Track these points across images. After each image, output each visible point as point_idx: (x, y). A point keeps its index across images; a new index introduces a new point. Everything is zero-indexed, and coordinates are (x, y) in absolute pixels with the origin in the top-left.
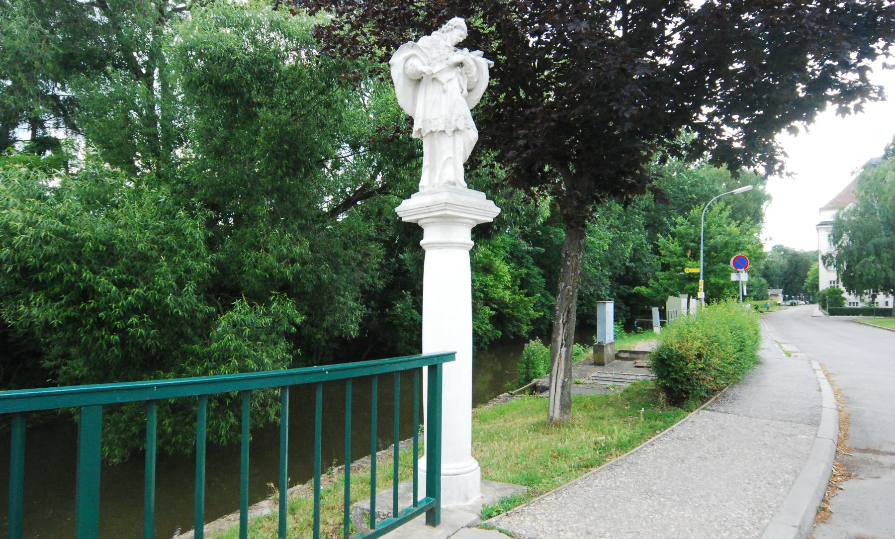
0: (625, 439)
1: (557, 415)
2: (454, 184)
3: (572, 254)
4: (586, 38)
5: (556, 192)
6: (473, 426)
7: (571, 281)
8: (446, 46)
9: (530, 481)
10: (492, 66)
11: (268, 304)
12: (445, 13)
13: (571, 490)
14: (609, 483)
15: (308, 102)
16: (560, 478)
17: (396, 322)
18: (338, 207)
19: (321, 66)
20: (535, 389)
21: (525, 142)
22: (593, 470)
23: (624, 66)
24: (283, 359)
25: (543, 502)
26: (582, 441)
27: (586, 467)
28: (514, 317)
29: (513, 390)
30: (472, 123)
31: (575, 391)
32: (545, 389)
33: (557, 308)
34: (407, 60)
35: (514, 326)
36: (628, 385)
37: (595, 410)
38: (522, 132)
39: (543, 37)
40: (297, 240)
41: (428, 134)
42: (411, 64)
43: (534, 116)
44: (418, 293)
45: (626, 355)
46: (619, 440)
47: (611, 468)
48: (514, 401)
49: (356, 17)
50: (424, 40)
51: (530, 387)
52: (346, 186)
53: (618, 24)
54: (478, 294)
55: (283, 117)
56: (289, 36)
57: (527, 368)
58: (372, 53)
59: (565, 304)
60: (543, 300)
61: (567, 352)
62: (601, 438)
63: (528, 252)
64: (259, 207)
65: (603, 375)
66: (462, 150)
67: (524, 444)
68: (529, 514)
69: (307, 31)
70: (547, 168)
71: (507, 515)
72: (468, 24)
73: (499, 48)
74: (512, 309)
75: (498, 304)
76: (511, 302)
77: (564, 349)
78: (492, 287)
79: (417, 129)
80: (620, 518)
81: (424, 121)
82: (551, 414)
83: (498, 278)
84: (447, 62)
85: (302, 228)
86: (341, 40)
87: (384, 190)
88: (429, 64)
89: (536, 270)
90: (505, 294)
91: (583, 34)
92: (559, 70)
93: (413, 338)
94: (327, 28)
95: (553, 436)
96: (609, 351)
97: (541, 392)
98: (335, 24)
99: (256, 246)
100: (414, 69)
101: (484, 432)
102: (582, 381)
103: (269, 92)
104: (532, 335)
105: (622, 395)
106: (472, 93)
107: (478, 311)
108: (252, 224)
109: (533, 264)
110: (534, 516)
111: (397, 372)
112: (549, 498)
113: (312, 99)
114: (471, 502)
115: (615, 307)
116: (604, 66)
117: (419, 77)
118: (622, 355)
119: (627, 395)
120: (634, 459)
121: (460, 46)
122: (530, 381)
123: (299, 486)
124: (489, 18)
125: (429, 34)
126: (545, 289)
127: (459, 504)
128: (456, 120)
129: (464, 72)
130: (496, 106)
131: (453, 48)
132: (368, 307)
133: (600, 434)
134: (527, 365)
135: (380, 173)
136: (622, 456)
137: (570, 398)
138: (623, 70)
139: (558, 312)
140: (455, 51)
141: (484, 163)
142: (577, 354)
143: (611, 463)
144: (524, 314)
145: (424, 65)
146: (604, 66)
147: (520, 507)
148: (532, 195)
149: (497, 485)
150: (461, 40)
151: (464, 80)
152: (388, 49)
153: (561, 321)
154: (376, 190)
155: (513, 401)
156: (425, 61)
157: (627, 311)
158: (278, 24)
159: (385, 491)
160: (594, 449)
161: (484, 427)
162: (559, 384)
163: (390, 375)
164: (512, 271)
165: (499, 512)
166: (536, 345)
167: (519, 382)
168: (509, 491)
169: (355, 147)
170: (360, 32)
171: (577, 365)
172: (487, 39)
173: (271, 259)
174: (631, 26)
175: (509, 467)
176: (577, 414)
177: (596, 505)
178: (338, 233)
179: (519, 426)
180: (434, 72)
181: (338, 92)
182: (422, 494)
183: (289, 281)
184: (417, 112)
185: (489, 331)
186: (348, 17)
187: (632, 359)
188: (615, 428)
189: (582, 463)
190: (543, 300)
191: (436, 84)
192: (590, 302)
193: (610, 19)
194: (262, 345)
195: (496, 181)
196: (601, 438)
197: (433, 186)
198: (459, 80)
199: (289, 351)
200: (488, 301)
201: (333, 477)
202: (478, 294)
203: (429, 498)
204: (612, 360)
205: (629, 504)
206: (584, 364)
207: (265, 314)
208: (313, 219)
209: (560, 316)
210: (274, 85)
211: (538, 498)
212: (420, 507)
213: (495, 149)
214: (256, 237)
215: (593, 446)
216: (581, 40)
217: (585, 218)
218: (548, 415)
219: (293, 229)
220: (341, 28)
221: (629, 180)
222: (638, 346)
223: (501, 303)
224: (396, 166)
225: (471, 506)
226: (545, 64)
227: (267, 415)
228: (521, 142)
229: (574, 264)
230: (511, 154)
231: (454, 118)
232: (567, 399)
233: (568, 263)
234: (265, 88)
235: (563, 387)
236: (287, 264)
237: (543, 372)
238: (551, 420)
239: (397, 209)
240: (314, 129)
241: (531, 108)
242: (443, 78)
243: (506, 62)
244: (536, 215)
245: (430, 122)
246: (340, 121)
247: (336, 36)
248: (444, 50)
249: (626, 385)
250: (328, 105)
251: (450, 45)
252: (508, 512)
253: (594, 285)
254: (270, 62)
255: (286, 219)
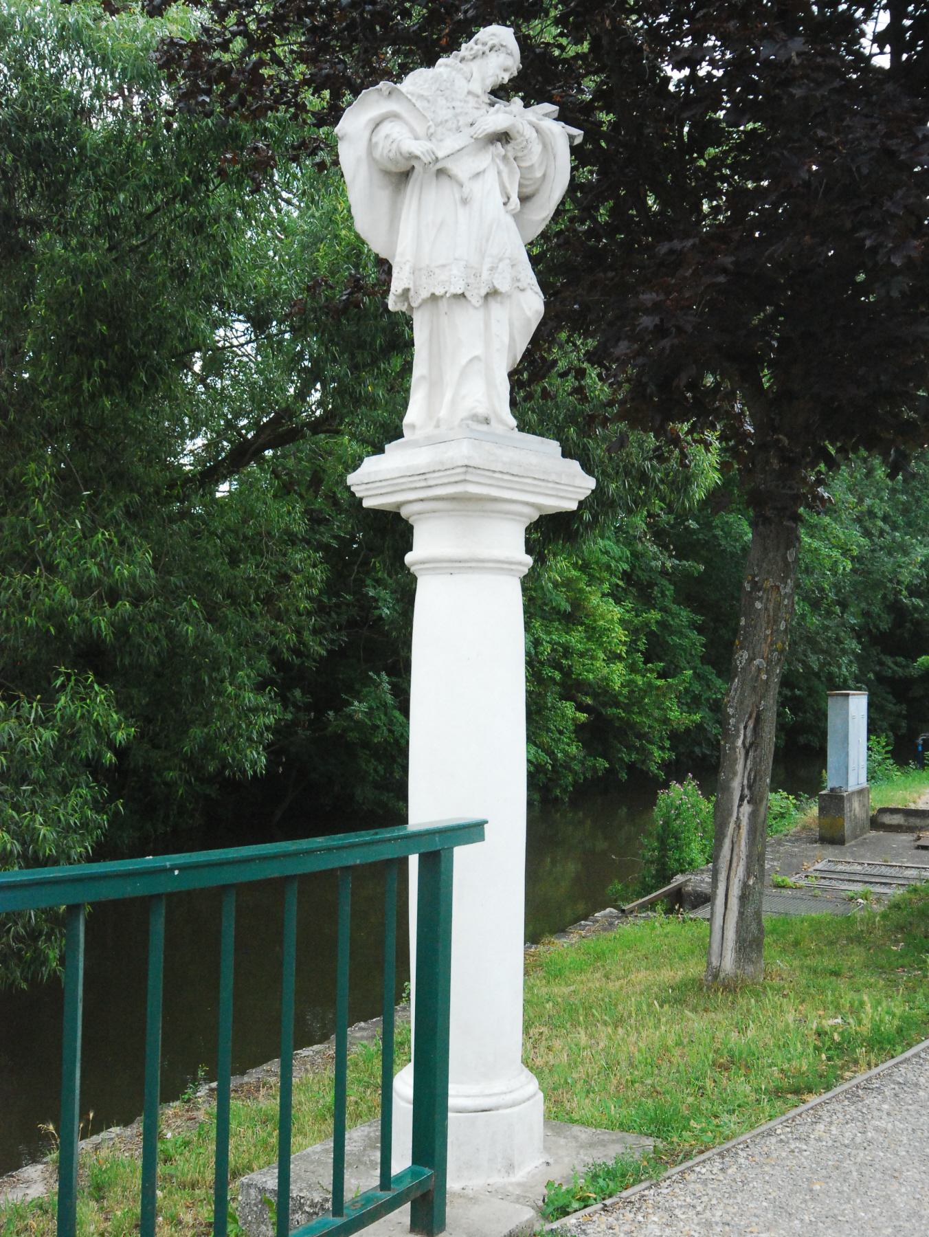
0: (890, 1025)
1: (728, 964)
2: (487, 421)
3: (768, 584)
4: (802, 77)
5: (732, 434)
6: (528, 988)
7: (765, 648)
8: (469, 93)
9: (660, 1125)
10: (578, 141)
11: (49, 700)
12: (471, 13)
13: (757, 1150)
14: (851, 1131)
15: (149, 216)
16: (734, 1118)
17: (353, 736)
18: (219, 464)
19: (179, 133)
20: (680, 901)
21: (657, 320)
22: (813, 1100)
23: (893, 143)
24: (85, 824)
25: (693, 1177)
26: (787, 1029)
27: (797, 1091)
28: (631, 726)
29: (628, 900)
30: (528, 276)
31: (771, 907)
32: (703, 899)
33: (731, 711)
34: (377, 125)
35: (630, 748)
36: (901, 891)
37: (821, 952)
38: (648, 297)
39: (704, 70)
40: (122, 543)
41: (425, 301)
42: (387, 136)
43: (676, 261)
44: (400, 669)
45: (897, 819)
46: (876, 1029)
47: (853, 1096)
48: (628, 928)
49: (260, 20)
50: (418, 80)
51: (668, 895)
52: (237, 416)
53: (879, 39)
54: (548, 672)
55: (92, 256)
56: (103, 61)
57: (663, 847)
58: (297, 105)
59: (749, 702)
60: (697, 688)
61: (753, 815)
62: (831, 1022)
63: (664, 572)
64: (33, 466)
65: (840, 867)
66: (506, 340)
67: (651, 1035)
68: (657, 1207)
69: (146, 49)
70: (709, 380)
71: (605, 1209)
72: (523, 40)
73: (598, 94)
74: (627, 708)
75: (595, 696)
76: (625, 691)
77: (746, 809)
78: (582, 655)
79: (400, 291)
80: (875, 1218)
81: (413, 272)
82: (715, 963)
83: (594, 634)
84: (472, 131)
85: (131, 515)
86: (226, 74)
87: (327, 424)
88: (430, 137)
89: (685, 615)
90: (612, 672)
91: (794, 66)
92: (740, 148)
93: (391, 773)
94: (191, 44)
95: (720, 1016)
96: (855, 809)
97: (695, 907)
98: (210, 37)
99: (24, 559)
100: (394, 146)
101: (556, 1004)
102: (790, 881)
103: (57, 195)
104: (675, 771)
105: (884, 916)
106: (529, 205)
107: (546, 713)
108: (16, 506)
109: (675, 601)
110: (669, 1210)
111: (346, 869)
112: (706, 1169)
113: (157, 210)
114: (520, 1175)
115: (870, 705)
116: (844, 143)
117: (404, 167)
118: (888, 819)
119: (894, 915)
120: (910, 1075)
121: (500, 92)
122: (668, 880)
123: (115, 1130)
124: (573, 26)
125: (430, 62)
126: (705, 659)
127: (491, 1181)
128: (492, 269)
129: (511, 155)
130: (589, 233)
131: (486, 98)
132: (285, 702)
133: (831, 1012)
134: (662, 841)
135: (318, 386)
136: (882, 1067)
137: (759, 923)
138: (891, 154)
139: (732, 721)
140: (492, 105)
141: (562, 365)
142: (782, 816)
143: (854, 1082)
144: (656, 720)
145: (416, 138)
146: (844, 143)
147: (637, 1188)
148: (675, 441)
149: (584, 1134)
150: (506, 78)
151: (511, 172)
152: (337, 96)
153: (739, 742)
154: (307, 425)
155: (627, 927)
156: (420, 130)
157: (899, 715)
158: (79, 33)
159: (318, 1147)
160: (816, 1048)
161: (556, 990)
162: (735, 891)
163: (328, 877)
164: (627, 616)
165: (585, 1202)
166: (685, 793)
167: (643, 883)
168: (610, 1152)
169: (259, 323)
170: (267, 57)
171: (779, 843)
172: (571, 72)
173: (62, 591)
174: (911, 46)
175: (612, 1089)
176: (778, 962)
177: (817, 1187)
178: (219, 528)
179: (638, 989)
180: (440, 155)
181: (220, 195)
182: (402, 1160)
183: (104, 641)
184: (399, 250)
185: (574, 758)
186: (241, 21)
187: (910, 829)
188: (866, 998)
189: (785, 1083)
190: (697, 688)
191: (444, 181)
192: (811, 691)
193: (863, 26)
194: (33, 792)
195: (587, 408)
196: (831, 1022)
197: (437, 426)
198: (499, 173)
199: (98, 807)
200: (572, 688)
201: (198, 1109)
202: (548, 672)
203: (418, 1168)
204: (863, 832)
205: (896, 1186)
206: (797, 839)
207: (40, 722)
208: (157, 493)
209: (738, 730)
210: (67, 178)
211: (679, 1168)
212: (397, 1189)
213: (587, 335)
214: (25, 536)
215: (812, 1040)
216: (787, 83)
217: (798, 499)
218: (709, 963)
219: (113, 516)
220: (225, 46)
221: (907, 414)
222: (924, 798)
223: (603, 692)
224: (355, 367)
225: (519, 1184)
226: (708, 133)
227: (42, 960)
228: (647, 321)
229: (771, 606)
230: (623, 348)
231: (486, 267)
232: (754, 927)
233: (758, 605)
234: (48, 185)
235: (743, 898)
236: (100, 598)
237: (700, 859)
238: (716, 976)
239: (351, 479)
240: (164, 284)
241: (671, 239)
242: (462, 169)
243: (614, 126)
244: (688, 480)
245: (430, 274)
246: (227, 265)
247: (212, 65)
248: (466, 102)
249: (896, 893)
250: (197, 227)
251: (479, 91)
252: (608, 1202)
253: (823, 652)
254: (59, 123)
255: (96, 494)
